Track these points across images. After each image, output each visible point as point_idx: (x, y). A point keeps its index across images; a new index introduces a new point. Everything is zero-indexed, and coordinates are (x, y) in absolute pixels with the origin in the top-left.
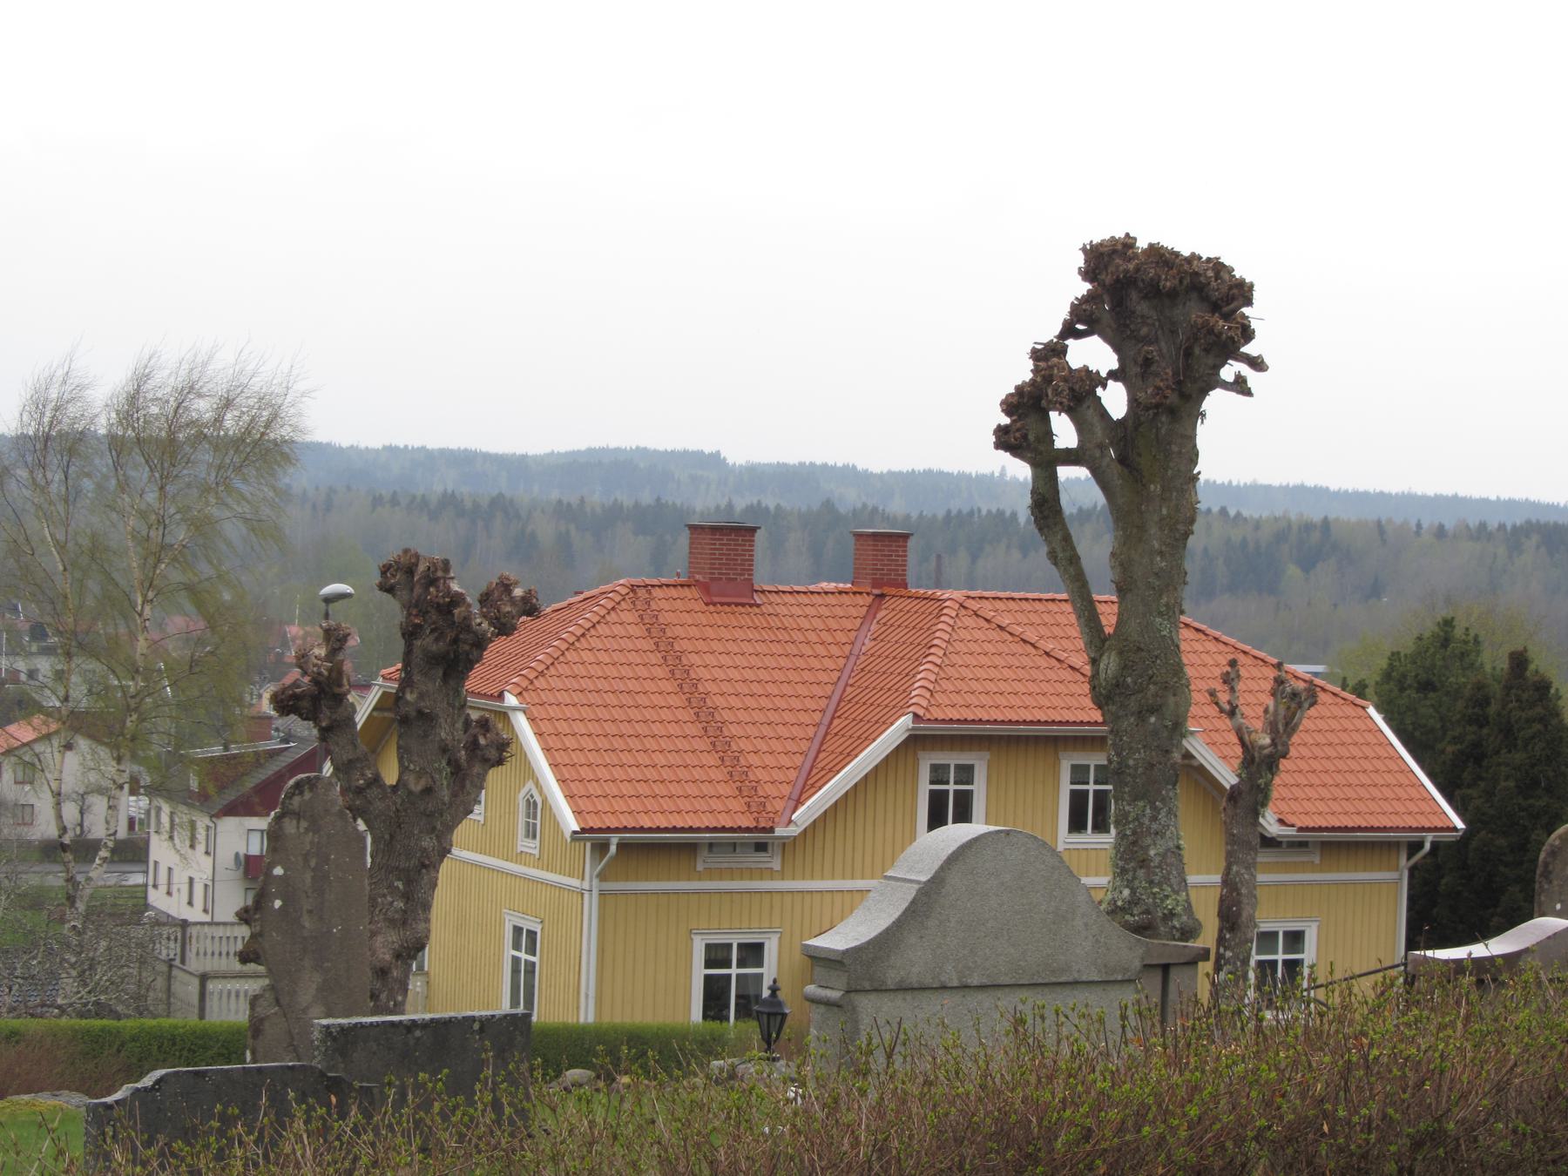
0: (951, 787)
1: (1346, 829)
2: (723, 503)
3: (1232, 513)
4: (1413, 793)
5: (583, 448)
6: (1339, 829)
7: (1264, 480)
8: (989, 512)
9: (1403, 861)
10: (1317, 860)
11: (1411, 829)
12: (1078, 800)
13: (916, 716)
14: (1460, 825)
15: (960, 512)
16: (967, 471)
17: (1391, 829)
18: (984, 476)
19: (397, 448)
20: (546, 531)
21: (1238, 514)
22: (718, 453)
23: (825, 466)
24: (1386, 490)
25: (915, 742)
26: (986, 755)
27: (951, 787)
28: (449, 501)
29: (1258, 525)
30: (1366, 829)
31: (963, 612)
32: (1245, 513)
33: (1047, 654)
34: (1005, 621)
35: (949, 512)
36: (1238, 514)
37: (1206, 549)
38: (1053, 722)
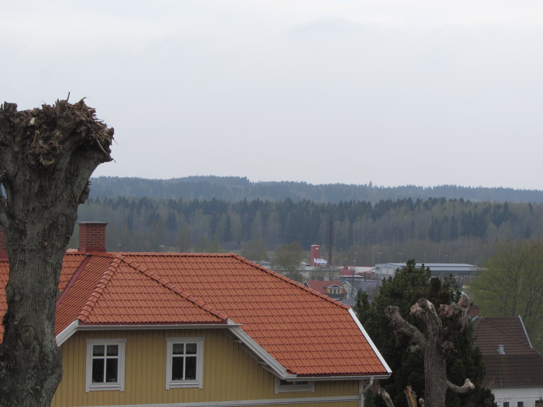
0: (105, 357)
1: (325, 374)
2: (242, 199)
3: (465, 200)
4: (367, 354)
5: (187, 176)
6: (321, 375)
7: (484, 186)
8: (359, 202)
9: (361, 390)
10: (313, 391)
11: (362, 374)
12: (177, 363)
13: (80, 322)
14: (389, 370)
15: (346, 202)
16: (355, 184)
17: (351, 374)
18: (362, 186)
19: (105, 177)
20: (164, 214)
21: (468, 202)
22: (246, 178)
23: (292, 183)
24: (538, 189)
25: (80, 335)
26: (125, 340)
27: (105, 357)
28: (122, 201)
29: (476, 206)
30: (337, 374)
31: (123, 264)
32: (472, 200)
33: (164, 286)
34: (143, 268)
35: (341, 202)
36: (468, 202)
37: (453, 217)
38: (158, 323)
